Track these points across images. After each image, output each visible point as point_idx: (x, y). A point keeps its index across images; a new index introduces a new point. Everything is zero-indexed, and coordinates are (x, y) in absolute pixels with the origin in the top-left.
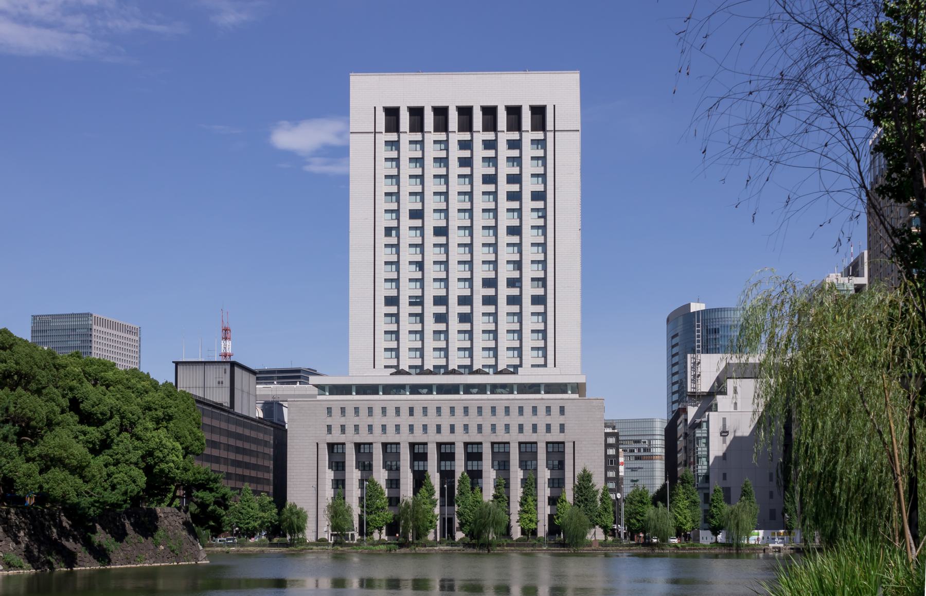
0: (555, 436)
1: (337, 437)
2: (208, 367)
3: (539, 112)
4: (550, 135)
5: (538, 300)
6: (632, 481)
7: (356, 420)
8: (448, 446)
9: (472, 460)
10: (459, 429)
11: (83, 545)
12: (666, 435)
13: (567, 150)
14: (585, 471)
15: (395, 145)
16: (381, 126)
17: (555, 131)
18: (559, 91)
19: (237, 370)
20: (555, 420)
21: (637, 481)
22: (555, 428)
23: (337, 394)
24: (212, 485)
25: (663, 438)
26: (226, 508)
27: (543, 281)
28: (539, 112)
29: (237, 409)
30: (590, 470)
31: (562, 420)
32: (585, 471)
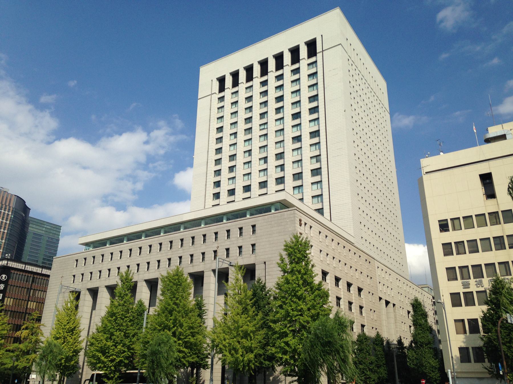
0: (246, 259)
1: (78, 286)
4: (319, 56)
5: (316, 172)
15: (221, 99)
18: (331, 27)
27: (318, 158)
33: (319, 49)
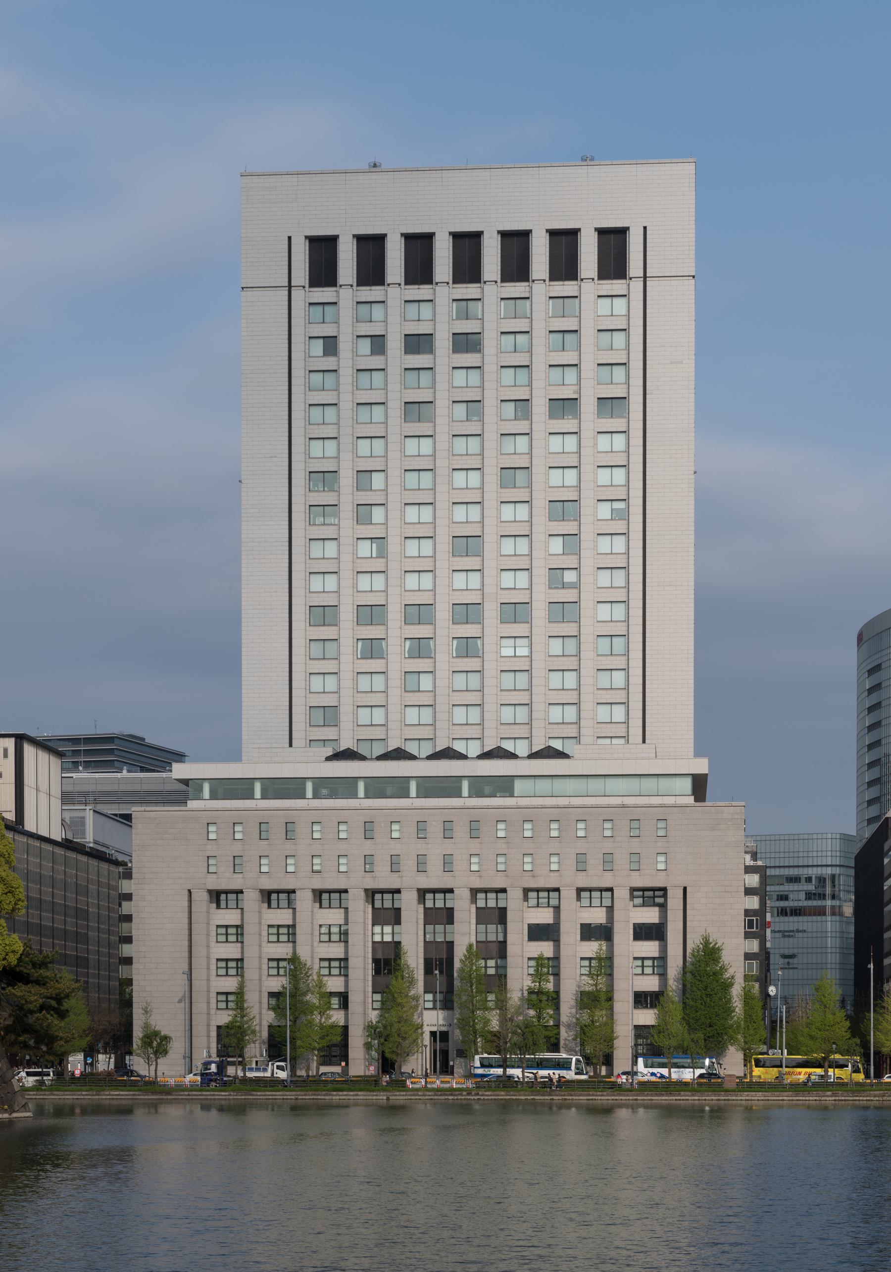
3: (613, 240)
6: (785, 956)
8: (388, 896)
9: (435, 923)
11: (848, 1017)
12: (857, 868)
13: (674, 312)
14: (706, 942)
16: (301, 274)
17: (645, 277)
18: (657, 201)
19: (29, 750)
21: (793, 956)
23: (276, 798)
24: (35, 974)
25: (852, 872)
26: (62, 1015)
28: (613, 240)
29: (30, 825)
30: (716, 937)
32: (706, 942)
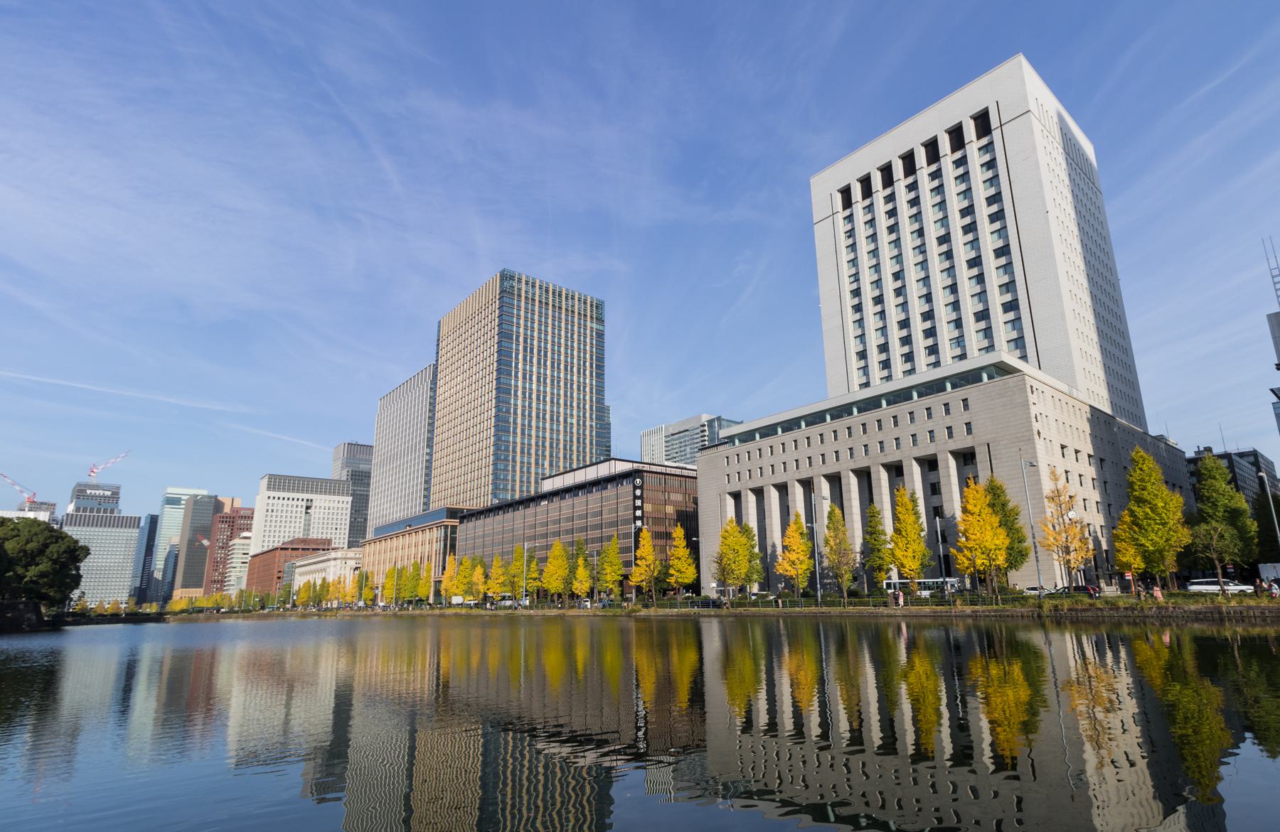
0: (962, 442)
2: (488, 501)
3: (982, 121)
4: (996, 134)
7: (896, 433)
10: (907, 441)
15: (850, 218)
20: (958, 418)
22: (960, 430)
31: (966, 417)
33: (994, 122)
